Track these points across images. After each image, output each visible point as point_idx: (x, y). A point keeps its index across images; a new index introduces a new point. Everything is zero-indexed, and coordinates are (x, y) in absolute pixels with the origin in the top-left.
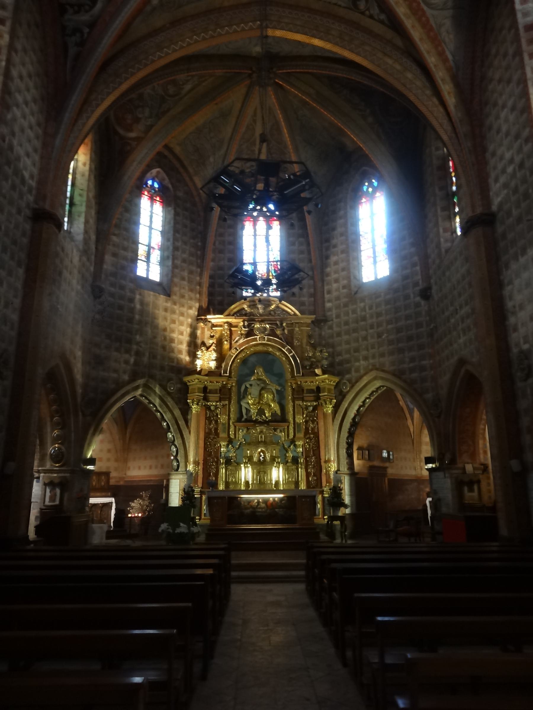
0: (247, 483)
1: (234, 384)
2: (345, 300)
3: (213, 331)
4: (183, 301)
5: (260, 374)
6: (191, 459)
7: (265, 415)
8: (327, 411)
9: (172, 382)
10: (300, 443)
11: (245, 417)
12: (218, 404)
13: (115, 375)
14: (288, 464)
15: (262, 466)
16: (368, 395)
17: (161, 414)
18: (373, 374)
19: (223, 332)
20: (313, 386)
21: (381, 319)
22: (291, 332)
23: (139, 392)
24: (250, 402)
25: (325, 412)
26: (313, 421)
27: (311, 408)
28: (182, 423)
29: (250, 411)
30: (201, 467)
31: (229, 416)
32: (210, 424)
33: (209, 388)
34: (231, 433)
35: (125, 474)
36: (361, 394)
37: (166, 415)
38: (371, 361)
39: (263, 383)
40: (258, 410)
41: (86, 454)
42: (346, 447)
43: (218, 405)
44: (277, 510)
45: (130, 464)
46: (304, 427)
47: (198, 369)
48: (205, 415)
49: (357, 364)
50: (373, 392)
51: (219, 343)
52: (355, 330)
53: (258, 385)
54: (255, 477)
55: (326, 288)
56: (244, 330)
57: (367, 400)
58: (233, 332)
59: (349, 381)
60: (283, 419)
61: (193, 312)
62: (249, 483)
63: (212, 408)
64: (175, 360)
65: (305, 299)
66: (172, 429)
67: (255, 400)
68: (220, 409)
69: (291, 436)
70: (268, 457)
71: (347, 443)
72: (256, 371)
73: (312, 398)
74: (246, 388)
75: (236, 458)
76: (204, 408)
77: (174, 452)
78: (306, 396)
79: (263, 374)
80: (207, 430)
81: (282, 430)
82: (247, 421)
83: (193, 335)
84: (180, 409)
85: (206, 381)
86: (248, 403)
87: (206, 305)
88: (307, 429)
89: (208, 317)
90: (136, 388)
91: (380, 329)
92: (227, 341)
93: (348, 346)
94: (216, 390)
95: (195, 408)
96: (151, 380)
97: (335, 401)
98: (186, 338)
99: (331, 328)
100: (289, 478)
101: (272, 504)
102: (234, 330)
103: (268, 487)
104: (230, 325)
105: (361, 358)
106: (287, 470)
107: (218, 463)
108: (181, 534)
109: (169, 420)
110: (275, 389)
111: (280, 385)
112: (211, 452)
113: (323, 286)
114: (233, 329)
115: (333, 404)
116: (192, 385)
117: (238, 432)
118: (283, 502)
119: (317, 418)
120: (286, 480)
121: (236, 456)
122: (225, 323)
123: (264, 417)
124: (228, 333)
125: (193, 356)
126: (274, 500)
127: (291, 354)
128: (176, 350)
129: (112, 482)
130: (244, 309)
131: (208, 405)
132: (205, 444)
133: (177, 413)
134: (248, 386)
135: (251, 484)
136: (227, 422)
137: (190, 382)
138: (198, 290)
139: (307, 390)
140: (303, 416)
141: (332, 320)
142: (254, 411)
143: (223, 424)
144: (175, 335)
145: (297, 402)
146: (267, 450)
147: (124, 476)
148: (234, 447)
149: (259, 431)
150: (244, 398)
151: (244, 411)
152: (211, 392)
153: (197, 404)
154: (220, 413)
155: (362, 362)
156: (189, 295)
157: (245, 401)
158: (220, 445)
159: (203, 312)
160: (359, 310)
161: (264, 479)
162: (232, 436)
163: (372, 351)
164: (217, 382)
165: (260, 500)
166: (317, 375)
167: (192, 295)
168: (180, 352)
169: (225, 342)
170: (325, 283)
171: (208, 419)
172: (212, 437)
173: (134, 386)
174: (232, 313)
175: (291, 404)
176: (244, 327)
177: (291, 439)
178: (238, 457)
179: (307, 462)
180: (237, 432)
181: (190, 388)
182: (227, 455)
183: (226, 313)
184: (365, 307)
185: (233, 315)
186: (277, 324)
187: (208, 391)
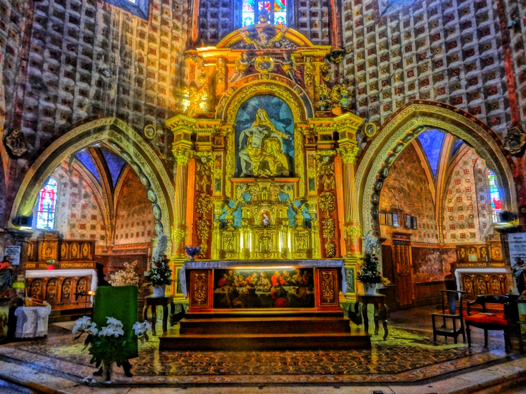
0: (247, 252)
2: (368, 23)
3: (205, 69)
4: (165, 28)
9: (150, 125)
10: (312, 202)
11: (244, 172)
13: (65, 108)
14: (298, 228)
15: (265, 231)
16: (411, 131)
19: (217, 69)
20: (330, 132)
21: (421, 36)
22: (301, 70)
23: (105, 136)
24: (250, 153)
25: (345, 162)
26: (329, 176)
27: (326, 160)
28: (165, 178)
29: (250, 164)
30: (189, 232)
31: (225, 170)
32: (201, 180)
33: (200, 134)
35: (114, 243)
38: (408, 93)
39: (266, 129)
46: (318, 183)
48: (194, 169)
50: (409, 135)
51: (213, 82)
52: (385, 57)
53: (260, 132)
55: (344, 13)
56: (243, 66)
58: (229, 69)
59: (377, 122)
61: (180, 45)
62: (249, 251)
63: (204, 160)
64: (156, 100)
65: (318, 30)
66: (153, 186)
67: (257, 151)
68: (214, 161)
69: (302, 194)
73: (329, 146)
74: (246, 137)
75: (233, 221)
80: (197, 188)
81: (291, 187)
82: (247, 176)
83: (180, 72)
84: (163, 161)
85: (195, 125)
86: (248, 155)
87: (197, 37)
88: (321, 187)
89: (199, 49)
90: (100, 130)
91: (422, 49)
92: (221, 79)
93: (374, 80)
94: (208, 137)
95: (181, 160)
96: (120, 121)
97: (358, 149)
98: (169, 74)
99: (351, 61)
102: (230, 67)
104: (226, 60)
105: (393, 91)
106: (297, 236)
108: (110, 338)
109: (148, 174)
110: (282, 137)
111: (287, 132)
112: (202, 214)
113: (340, 11)
114: (228, 65)
115: (356, 153)
117: (236, 189)
119: (334, 171)
120: (296, 248)
122: (218, 57)
123: (268, 171)
124: (223, 69)
125: (177, 95)
127: (302, 94)
129: (98, 252)
130: (241, 41)
131: (198, 156)
132: (195, 204)
133: (159, 165)
136: (222, 177)
137: (174, 127)
138: (186, 20)
139: (321, 136)
141: (353, 51)
142: (255, 165)
143: (217, 180)
144: (155, 69)
145: (308, 153)
147: (112, 245)
148: (230, 208)
150: (243, 148)
151: (243, 165)
153: (184, 154)
154: (213, 167)
156: (174, 23)
157: (244, 152)
158: (214, 205)
159: (192, 44)
160: (389, 30)
161: (268, 247)
162: (228, 194)
163: (408, 81)
165: (262, 274)
166: (334, 116)
167: (179, 24)
168: (162, 90)
169: (220, 81)
170: (343, 8)
171: (198, 174)
172: (203, 195)
174: (228, 45)
176: (243, 61)
177: (302, 198)
179: (322, 226)
180: (234, 190)
182: (222, 217)
183: (221, 43)
184: (398, 25)
185: (231, 46)
186: (283, 59)
187: (197, 138)
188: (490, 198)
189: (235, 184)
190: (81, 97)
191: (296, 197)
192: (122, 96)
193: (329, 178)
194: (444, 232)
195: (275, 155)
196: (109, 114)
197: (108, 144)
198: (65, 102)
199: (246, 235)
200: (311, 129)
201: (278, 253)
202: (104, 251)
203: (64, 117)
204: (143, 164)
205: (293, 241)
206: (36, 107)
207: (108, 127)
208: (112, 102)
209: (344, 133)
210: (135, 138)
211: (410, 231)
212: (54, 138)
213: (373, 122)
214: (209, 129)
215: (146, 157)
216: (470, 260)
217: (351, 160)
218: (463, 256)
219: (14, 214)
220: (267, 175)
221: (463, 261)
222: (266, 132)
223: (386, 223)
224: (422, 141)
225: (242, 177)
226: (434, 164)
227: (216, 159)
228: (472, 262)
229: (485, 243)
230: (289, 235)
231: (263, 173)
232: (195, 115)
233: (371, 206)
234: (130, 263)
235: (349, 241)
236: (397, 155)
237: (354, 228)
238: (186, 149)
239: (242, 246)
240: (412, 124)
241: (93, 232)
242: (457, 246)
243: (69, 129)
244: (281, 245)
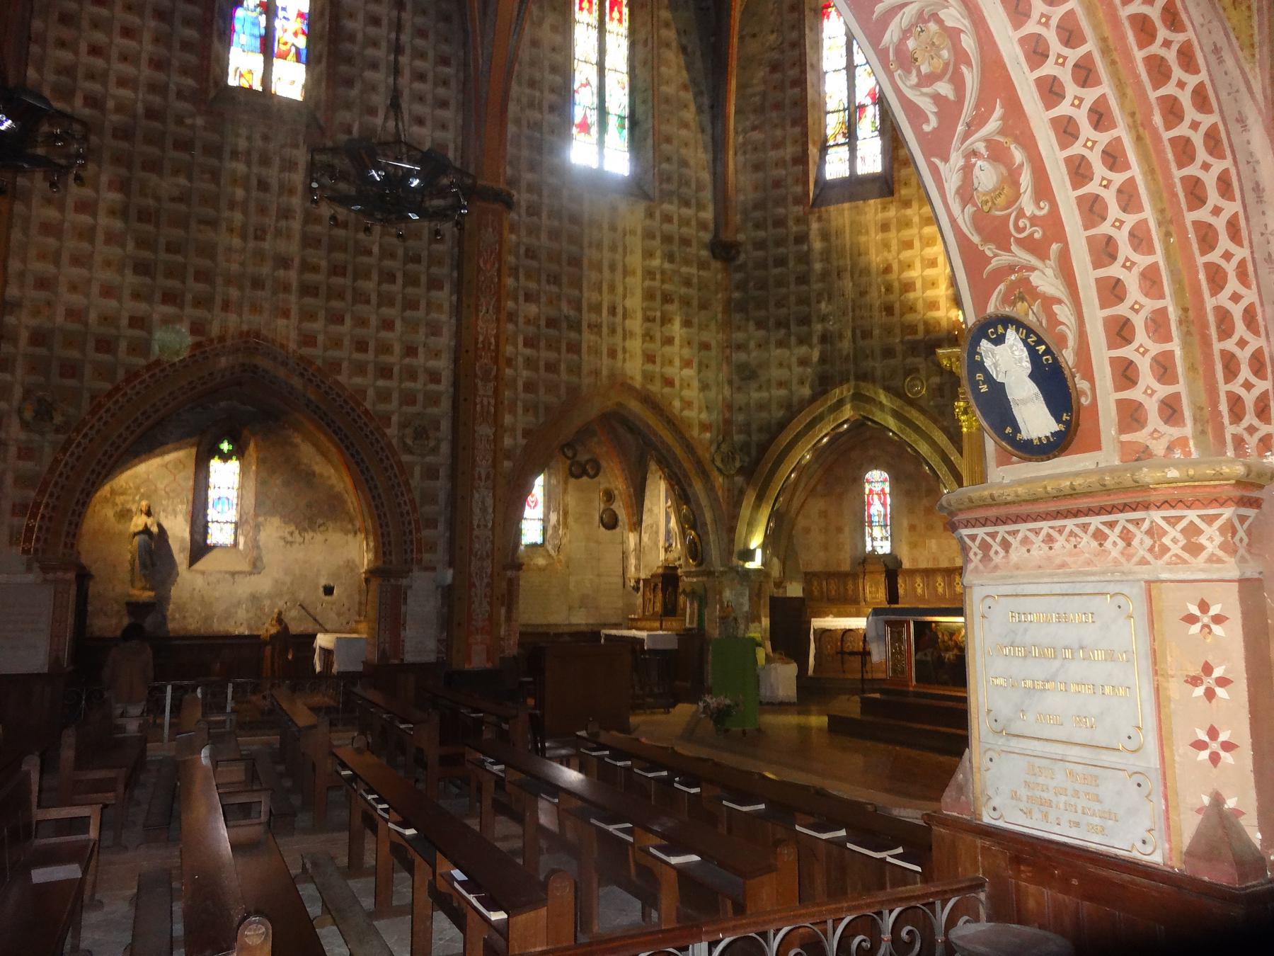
23: (848, 412)
90: (840, 403)
96: (862, 384)
128: (920, 305)
133: (941, 439)
144: (914, 274)
168: (933, 305)
190: (800, 369)
192: (861, 343)
196: (844, 380)
198: (781, 384)
203: (782, 406)
206: (748, 404)
207: (848, 400)
208: (847, 358)
210: (893, 404)
212: (773, 437)
219: (736, 549)
243: (789, 420)
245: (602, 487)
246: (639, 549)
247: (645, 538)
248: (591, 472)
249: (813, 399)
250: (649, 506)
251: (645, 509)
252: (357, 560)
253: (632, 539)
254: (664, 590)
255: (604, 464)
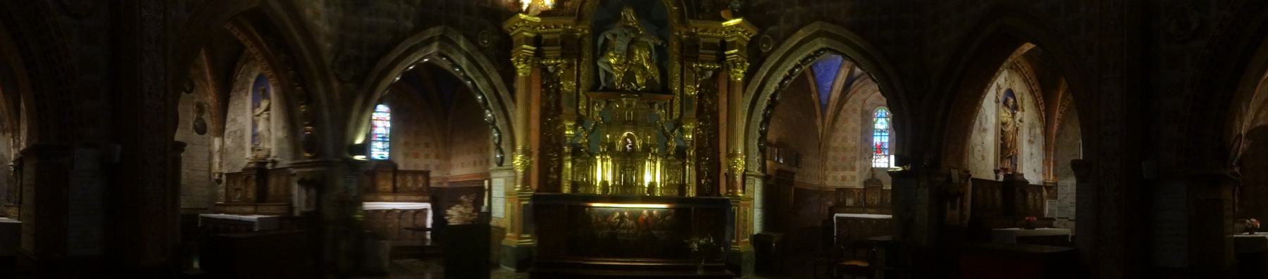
0: (604, 183)
1: (586, 32)
5: (629, 18)
6: (519, 148)
7: (635, 83)
8: (735, 78)
9: (484, 31)
10: (689, 126)
11: (603, 84)
12: (559, 61)
14: (669, 158)
16: (800, 61)
17: (473, 83)
18: (816, 26)
23: (434, 48)
24: (612, 61)
27: (710, 73)
28: (504, 93)
29: (612, 75)
30: (535, 159)
33: (545, 37)
34: (580, 107)
36: (790, 57)
37: (479, 83)
39: (633, 32)
40: (625, 73)
41: (354, 139)
42: (758, 137)
43: (559, 64)
44: (654, 232)
45: (454, 161)
46: (697, 103)
47: (524, 8)
49: (789, 10)
50: (810, 56)
54: (617, 175)
57: (797, 70)
60: (665, 89)
62: (608, 184)
63: (550, 69)
66: (490, 104)
67: (620, 58)
69: (676, 114)
70: (640, 145)
71: (761, 132)
72: (622, 14)
74: (606, 40)
75: (589, 146)
76: (538, 70)
77: (494, 138)
78: (702, 54)
79: (634, 18)
80: (544, 105)
82: (605, 89)
84: (500, 72)
86: (609, 63)
90: (429, 42)
94: (555, 40)
95: (522, 69)
97: (748, 64)
100: (670, 179)
101: (646, 221)
103: (637, 192)
106: (667, 167)
107: (561, 154)
109: (484, 89)
110: (654, 43)
111: (660, 38)
116: (516, 34)
118: (667, 218)
121: (588, 144)
126: (650, 214)
129: (433, 183)
133: (496, 78)
134: (608, 36)
135: (611, 186)
136: (575, 91)
137: (513, 30)
140: (695, 86)
142: (618, 77)
146: (637, 134)
147: (448, 176)
148: (585, 130)
149: (625, 103)
150: (602, 55)
152: (548, 43)
153: (525, 62)
155: (798, 8)
157: (604, 60)
161: (632, 180)
162: (583, 113)
164: (556, 27)
165: (626, 213)
173: (426, 37)
175: (677, 66)
178: (591, 144)
181: (515, 39)
182: (574, 142)
187: (543, 42)
188: (873, 142)
189: (591, 99)
191: (668, 119)
193: (711, 98)
194: (826, 172)
195: (645, 65)
197: (437, 58)
199: (605, 163)
200: (692, 34)
201: (644, 187)
202: (439, 183)
204: (476, 78)
205: (663, 174)
209: (734, 42)
211: (795, 169)
213: (770, 35)
214: (557, 30)
215: (480, 69)
216: (847, 205)
217: (740, 77)
218: (841, 200)
220: (632, 89)
221: (841, 207)
222: (633, 35)
223: (772, 159)
224: (816, 70)
225: (600, 91)
226: (824, 97)
227: (566, 68)
228: (848, 207)
229: (863, 187)
230: (658, 165)
231: (628, 87)
232: (539, 12)
233: (758, 135)
234: (468, 197)
235: (730, 176)
236: (793, 78)
237: (738, 161)
238: (528, 56)
239: (599, 180)
240: (815, 45)
241: (427, 162)
242: (837, 189)
244: (648, 179)
245: (196, 100)
246: (223, 151)
247: (228, 142)
248: (188, 89)
249: (415, 31)
250: (233, 117)
251: (229, 119)
252: (6, 154)
253: (217, 142)
254: (257, 181)
255: (197, 83)
